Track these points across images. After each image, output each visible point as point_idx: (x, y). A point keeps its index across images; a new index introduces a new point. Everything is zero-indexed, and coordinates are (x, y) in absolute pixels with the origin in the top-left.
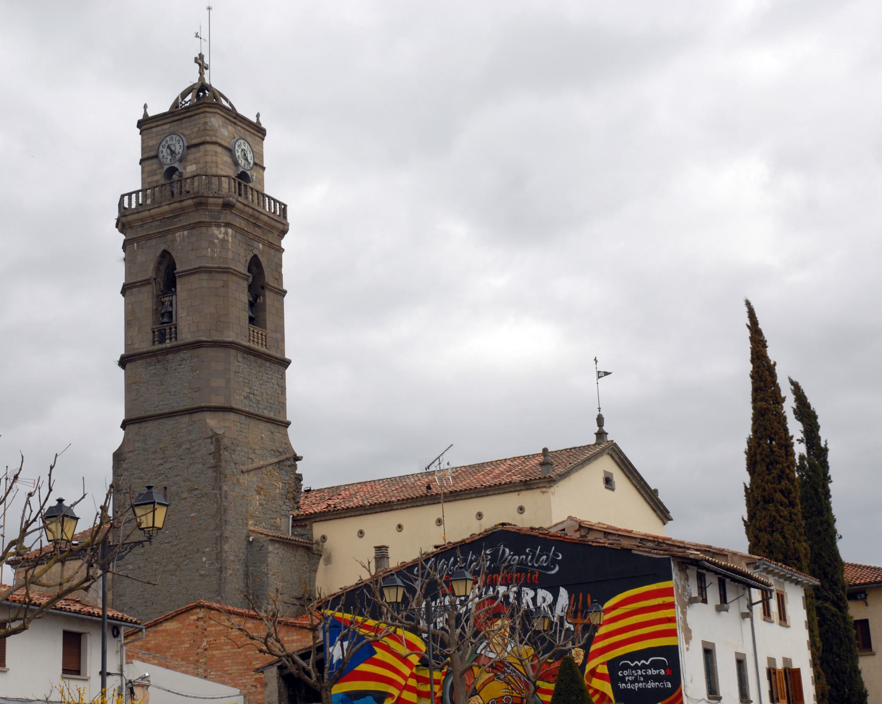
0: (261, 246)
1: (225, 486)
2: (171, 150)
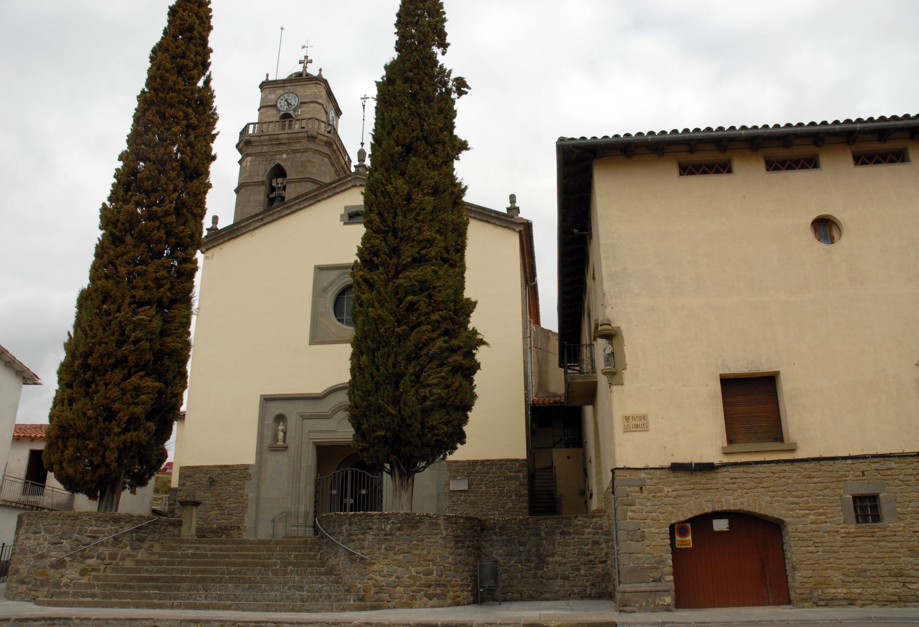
0: (285, 156)
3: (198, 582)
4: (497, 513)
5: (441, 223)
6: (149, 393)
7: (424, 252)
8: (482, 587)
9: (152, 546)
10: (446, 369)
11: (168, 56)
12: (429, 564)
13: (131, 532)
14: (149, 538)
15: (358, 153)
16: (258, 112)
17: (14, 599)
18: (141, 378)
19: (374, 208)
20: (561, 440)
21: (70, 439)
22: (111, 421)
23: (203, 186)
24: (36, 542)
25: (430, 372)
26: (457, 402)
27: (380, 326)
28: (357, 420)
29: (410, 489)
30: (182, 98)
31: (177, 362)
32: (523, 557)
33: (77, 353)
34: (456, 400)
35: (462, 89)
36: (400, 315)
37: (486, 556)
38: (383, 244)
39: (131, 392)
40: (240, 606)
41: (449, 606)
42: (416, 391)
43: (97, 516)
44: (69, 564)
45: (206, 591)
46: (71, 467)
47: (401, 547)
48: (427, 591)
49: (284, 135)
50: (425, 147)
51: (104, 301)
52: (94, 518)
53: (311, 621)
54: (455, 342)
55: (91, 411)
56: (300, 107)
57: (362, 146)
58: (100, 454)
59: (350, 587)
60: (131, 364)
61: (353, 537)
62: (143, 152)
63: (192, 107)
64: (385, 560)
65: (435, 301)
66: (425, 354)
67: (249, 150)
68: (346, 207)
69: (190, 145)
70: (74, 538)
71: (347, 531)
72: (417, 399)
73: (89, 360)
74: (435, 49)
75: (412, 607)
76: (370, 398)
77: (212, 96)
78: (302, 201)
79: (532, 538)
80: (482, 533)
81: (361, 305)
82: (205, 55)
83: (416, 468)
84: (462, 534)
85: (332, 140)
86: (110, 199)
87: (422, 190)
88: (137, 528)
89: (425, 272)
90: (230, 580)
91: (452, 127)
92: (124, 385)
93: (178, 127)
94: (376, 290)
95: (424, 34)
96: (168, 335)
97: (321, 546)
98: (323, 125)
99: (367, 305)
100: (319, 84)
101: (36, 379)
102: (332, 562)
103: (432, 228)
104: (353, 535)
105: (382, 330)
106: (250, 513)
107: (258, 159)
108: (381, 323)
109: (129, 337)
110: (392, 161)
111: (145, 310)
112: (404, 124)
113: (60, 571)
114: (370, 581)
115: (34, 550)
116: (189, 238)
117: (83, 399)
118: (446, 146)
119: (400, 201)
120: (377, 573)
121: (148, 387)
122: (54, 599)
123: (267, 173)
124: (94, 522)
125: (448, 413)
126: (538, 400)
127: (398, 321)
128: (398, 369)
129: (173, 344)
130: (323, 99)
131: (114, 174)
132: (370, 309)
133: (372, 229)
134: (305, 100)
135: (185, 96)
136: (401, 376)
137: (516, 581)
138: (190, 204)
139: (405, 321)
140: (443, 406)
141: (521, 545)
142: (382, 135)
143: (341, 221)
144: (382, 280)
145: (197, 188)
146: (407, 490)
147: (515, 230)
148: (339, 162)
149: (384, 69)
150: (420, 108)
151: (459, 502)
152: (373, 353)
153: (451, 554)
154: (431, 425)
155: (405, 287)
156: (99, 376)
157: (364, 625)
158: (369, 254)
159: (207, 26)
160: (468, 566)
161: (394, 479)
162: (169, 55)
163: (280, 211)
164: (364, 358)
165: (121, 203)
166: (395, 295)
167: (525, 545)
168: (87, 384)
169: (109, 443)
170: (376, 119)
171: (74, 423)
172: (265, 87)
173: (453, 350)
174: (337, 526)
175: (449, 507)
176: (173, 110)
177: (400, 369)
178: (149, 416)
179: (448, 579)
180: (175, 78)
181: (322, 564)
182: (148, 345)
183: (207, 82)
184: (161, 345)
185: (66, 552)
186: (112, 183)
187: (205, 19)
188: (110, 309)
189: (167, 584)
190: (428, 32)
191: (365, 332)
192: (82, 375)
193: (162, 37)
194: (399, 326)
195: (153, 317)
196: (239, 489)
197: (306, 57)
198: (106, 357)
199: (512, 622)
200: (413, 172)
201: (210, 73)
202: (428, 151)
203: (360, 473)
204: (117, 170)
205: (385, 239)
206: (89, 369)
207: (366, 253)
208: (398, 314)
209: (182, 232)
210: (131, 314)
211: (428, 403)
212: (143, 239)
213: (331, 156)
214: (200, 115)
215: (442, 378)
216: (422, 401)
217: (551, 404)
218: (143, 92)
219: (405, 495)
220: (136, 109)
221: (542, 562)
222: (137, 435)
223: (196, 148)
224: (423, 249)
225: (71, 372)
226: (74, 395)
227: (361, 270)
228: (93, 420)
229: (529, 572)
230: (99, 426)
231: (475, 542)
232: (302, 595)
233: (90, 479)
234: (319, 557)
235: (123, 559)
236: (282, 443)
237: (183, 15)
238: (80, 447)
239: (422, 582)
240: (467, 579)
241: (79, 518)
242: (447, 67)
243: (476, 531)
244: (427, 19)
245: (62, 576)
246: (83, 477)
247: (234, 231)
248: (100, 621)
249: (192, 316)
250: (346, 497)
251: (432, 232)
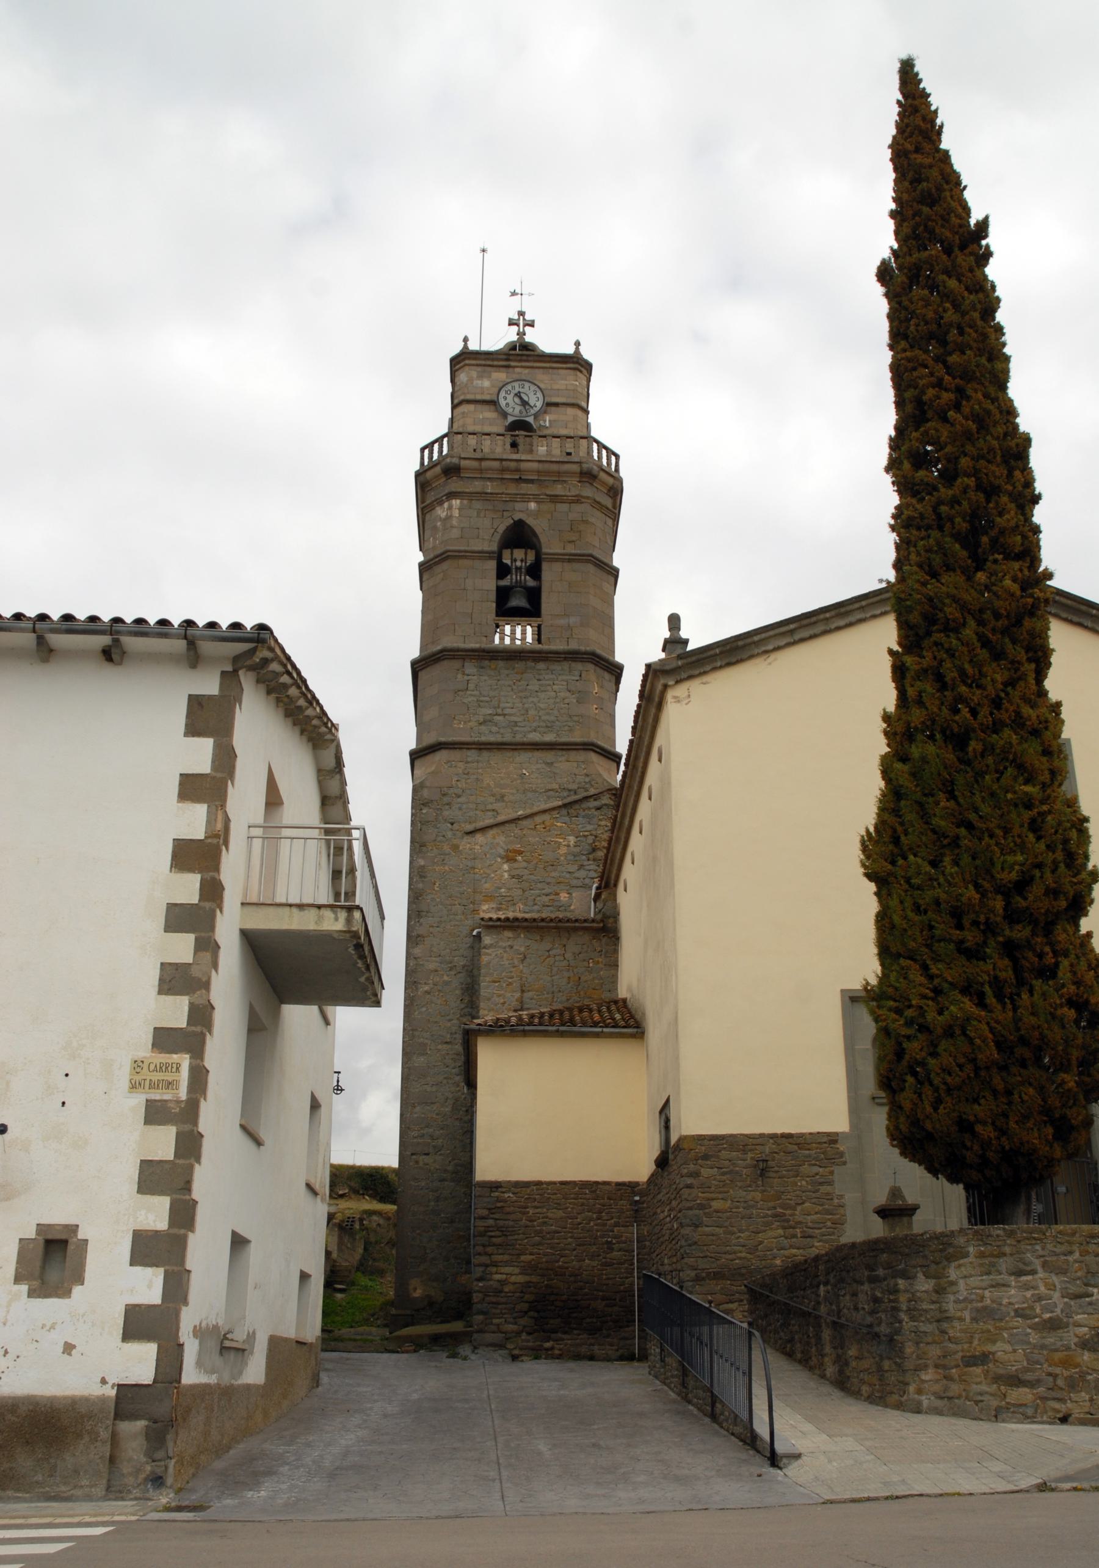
0: (533, 505)
2: (521, 398)
56: (545, 412)
78: (872, 604)
100: (581, 372)
107: (477, 505)
115: (1028, 1312)
172: (467, 362)
196: (821, 1184)
197: (521, 314)
247: (737, 648)
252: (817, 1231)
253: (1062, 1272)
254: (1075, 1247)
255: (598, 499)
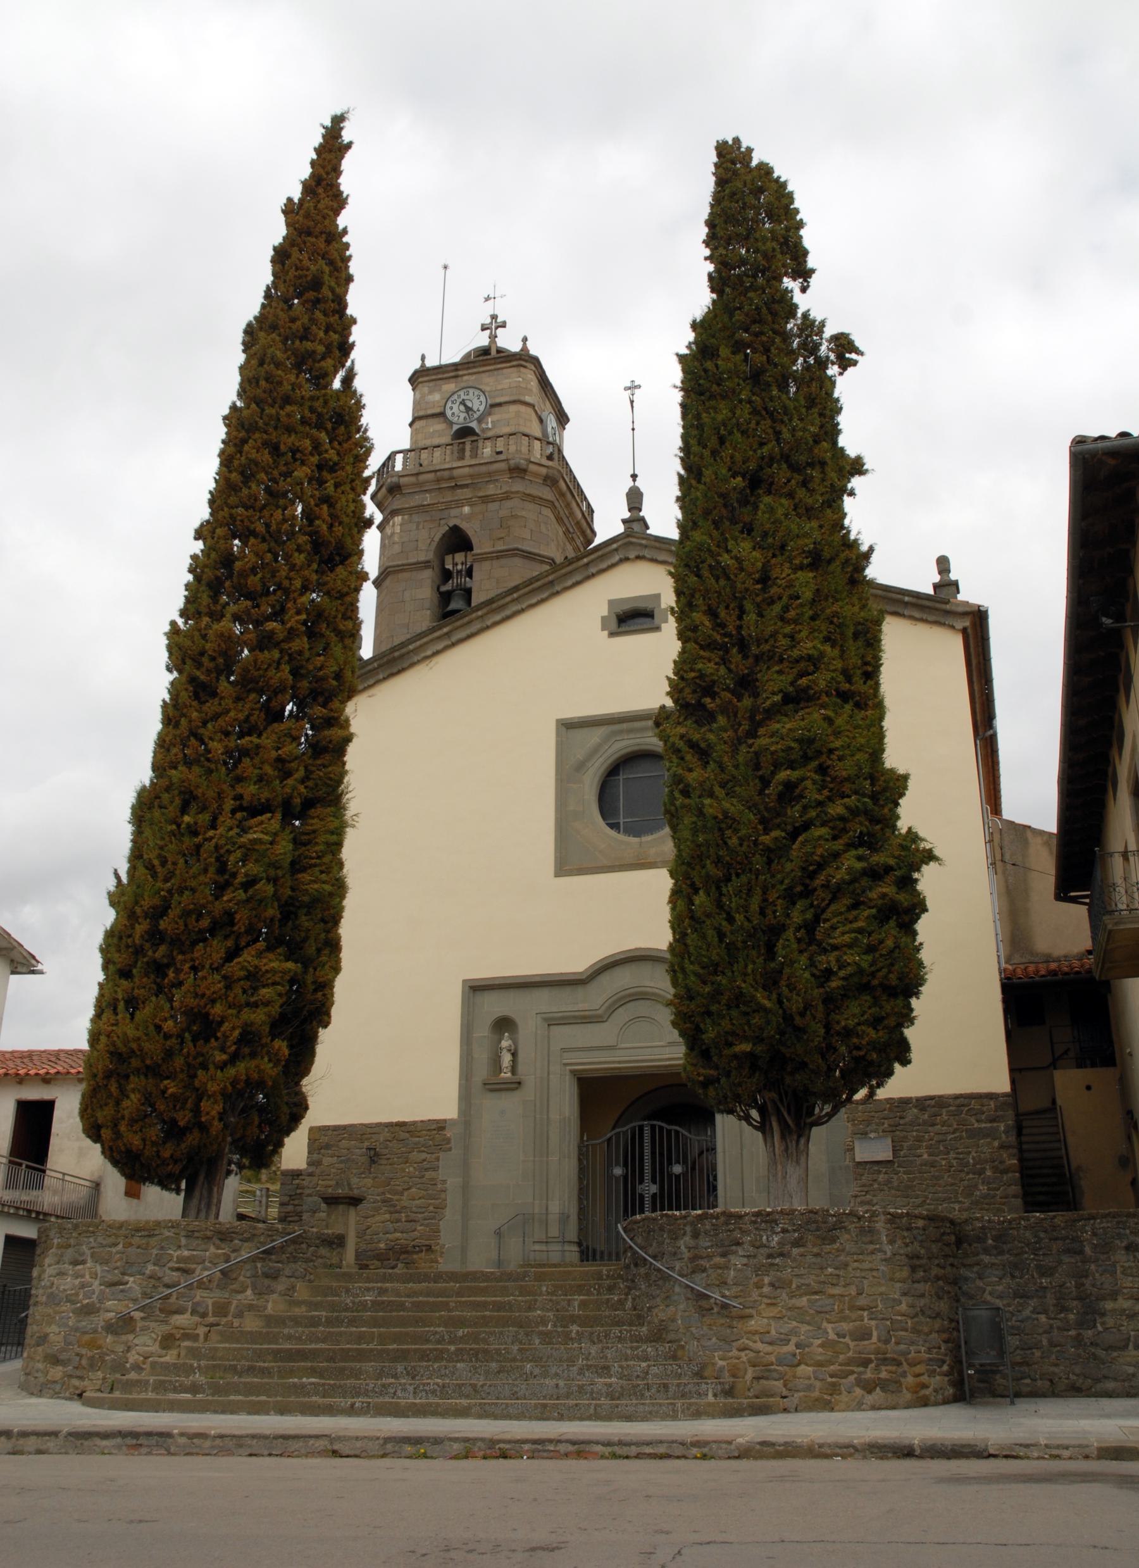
1: (935, 1251)
2: (465, 406)
3: (395, 1360)
4: (957, 1206)
5: (832, 623)
6: (274, 984)
7: (804, 681)
8: (970, 1366)
9: (293, 1287)
10: (866, 913)
11: (278, 338)
12: (862, 1316)
13: (253, 1260)
14: (287, 1272)
15: (628, 495)
16: (409, 430)
17: (40, 1394)
18: (260, 955)
19: (699, 601)
20: (1066, 1052)
21: (132, 1077)
22: (207, 1041)
23: (353, 578)
24: (77, 1282)
25: (835, 920)
26: (893, 979)
27: (728, 833)
28: (692, 1022)
29: (803, 1159)
30: (307, 413)
31: (323, 920)
32: (1050, 1300)
33: (138, 910)
34: (891, 976)
35: (847, 355)
36: (767, 809)
37: (971, 1297)
38: (723, 671)
39: (242, 982)
40: (487, 1408)
41: (908, 1406)
42: (810, 959)
43: (190, 1228)
44: (140, 1324)
45: (413, 1378)
46: (136, 1132)
47: (803, 1281)
48: (860, 1373)
49: (463, 468)
50: (789, 474)
51: (184, 810)
52: (183, 1233)
53: (648, 1439)
54: (879, 858)
55: (170, 1023)
56: (490, 414)
57: (634, 480)
58: (189, 1105)
59: (703, 1367)
60: (240, 927)
61: (702, 1262)
62: (242, 521)
63: (326, 429)
64: (772, 1308)
65: (834, 779)
66: (823, 886)
67: (398, 503)
68: (611, 603)
69: (327, 500)
70: (148, 1272)
71: (689, 1249)
72: (813, 975)
73: (161, 922)
74: (788, 283)
75: (832, 1410)
76: (719, 978)
77: (359, 406)
79: (1066, 1259)
80: (958, 1249)
81: (686, 793)
82: (344, 329)
83: (814, 1118)
84: (922, 1251)
85: (556, 473)
86: (183, 613)
87: (790, 560)
88: (264, 1252)
89: (811, 719)
90: (459, 1355)
91: (835, 431)
92: (228, 968)
93: (304, 468)
94: (715, 761)
95: (765, 256)
96: (304, 869)
97: (633, 1281)
98: (537, 444)
99: (698, 793)
100: (525, 367)
101: (34, 962)
102: (661, 1313)
103: (816, 634)
104: (702, 1258)
105: (734, 841)
106: (450, 1218)
107: (416, 518)
108: (730, 827)
109: (234, 875)
110: (725, 506)
111: (262, 823)
112: (743, 433)
113: (124, 1338)
114: (743, 1354)
116: (334, 679)
117: (154, 999)
118: (828, 469)
119: (749, 583)
120: (757, 1338)
121: (273, 971)
122: (117, 1394)
123: (434, 545)
124: (183, 1241)
125: (876, 1002)
126: (1014, 970)
127: (763, 821)
128: (771, 916)
129: (316, 886)
130: (534, 395)
131: (187, 566)
132: (707, 801)
133: (696, 642)
134: (498, 400)
135: (312, 410)
136: (777, 930)
137: (1038, 1353)
138: (333, 613)
139: (778, 821)
140: (865, 988)
141: (1042, 1275)
142: (702, 457)
143: (603, 629)
144: (725, 743)
145: (344, 581)
146: (798, 1162)
147: (953, 627)
148: (572, 513)
149: (690, 330)
150: (771, 399)
151: (876, 1186)
152: (718, 888)
153: (904, 1294)
154: (845, 1028)
155: (773, 753)
156: (183, 953)
157: (758, 1447)
158: (694, 692)
159: (344, 276)
160: (939, 1320)
161: (769, 1139)
162: (280, 335)
163: (481, 616)
164: (700, 899)
165: (206, 620)
166: (754, 770)
167: (1052, 1275)
168: (159, 969)
169: (206, 1084)
170: (684, 427)
171: (139, 1045)
172: (421, 380)
173: (876, 874)
174: (667, 1241)
175: (856, 1196)
176: (293, 436)
177: (775, 917)
178: (277, 1026)
179: (902, 1347)
180: (293, 378)
181: (640, 1320)
182: (270, 889)
183: (348, 380)
184: (293, 889)
185: (135, 1300)
186: (185, 582)
187: (340, 264)
188: (196, 823)
189: (333, 1365)
190: (774, 250)
191: (699, 846)
192: (150, 953)
193: (263, 304)
194: (766, 831)
195: (275, 834)
196: (427, 1170)
197: (494, 317)
198: (194, 916)
199: (1073, 1442)
200: (768, 526)
201: (353, 362)
202: (793, 482)
203: (669, 1132)
204: (194, 557)
205: (724, 661)
206: (162, 940)
207: (687, 690)
208: (762, 807)
209: (321, 669)
210: (236, 830)
211: (834, 984)
212: (250, 686)
213: (557, 504)
214: (340, 444)
215: (860, 931)
216: (823, 980)
217: (1043, 976)
218: (234, 407)
219: (794, 1173)
220: (223, 442)
221: (1090, 1313)
222: (257, 1066)
223: (338, 506)
224: (801, 675)
225: (128, 946)
226: (136, 991)
227: (679, 723)
228: (174, 1040)
229: (1066, 1333)
230: (185, 1050)
231: (949, 1269)
232: (610, 1385)
233: (172, 1156)
234: (629, 1304)
235: (240, 1315)
236: (509, 1075)
237: (301, 261)
238: (150, 1094)
239: (850, 1354)
240: (940, 1348)
241: (156, 1232)
242: (817, 315)
243: (948, 1245)
244: (767, 226)
245: (129, 1349)
246: (158, 1151)
247: (395, 660)
248: (227, 1440)
249: (347, 830)
250: (641, 1181)
251: (816, 642)
252: (420, 1216)
253: (106, 1262)
254: (121, 1240)
255: (527, 492)
